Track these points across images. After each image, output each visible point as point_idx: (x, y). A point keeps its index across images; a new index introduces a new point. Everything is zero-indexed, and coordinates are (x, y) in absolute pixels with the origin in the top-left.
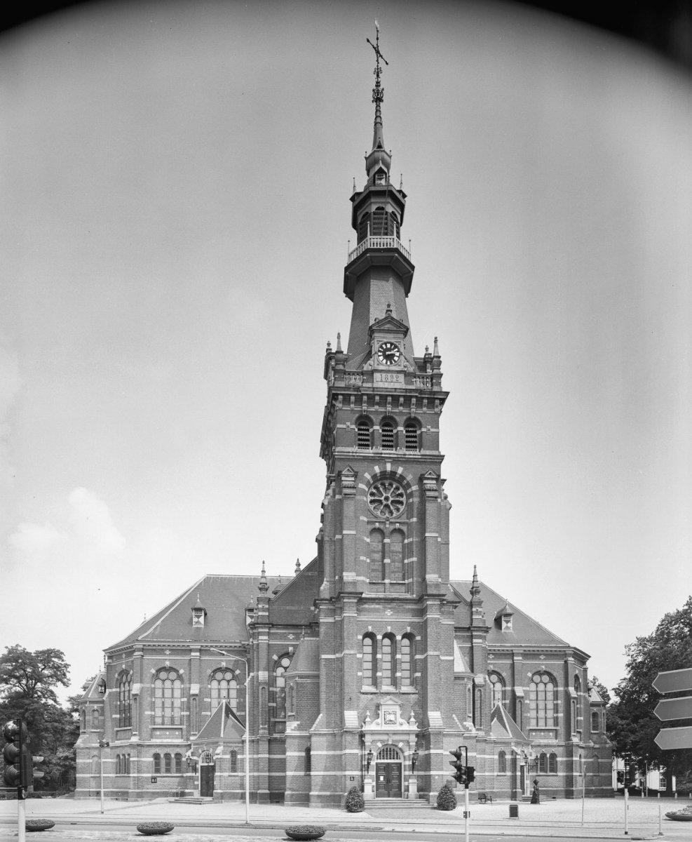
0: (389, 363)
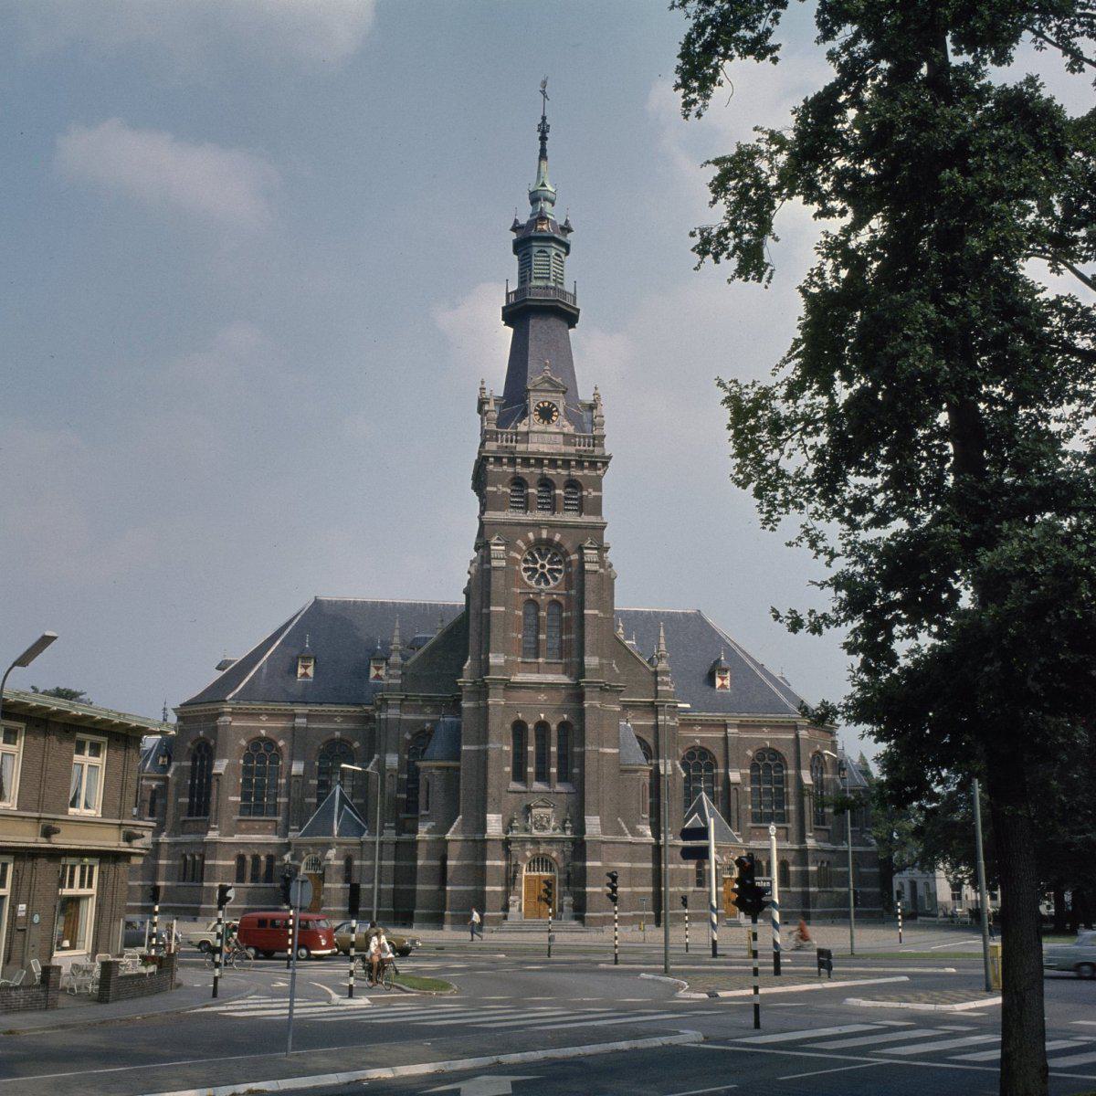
0: (546, 423)
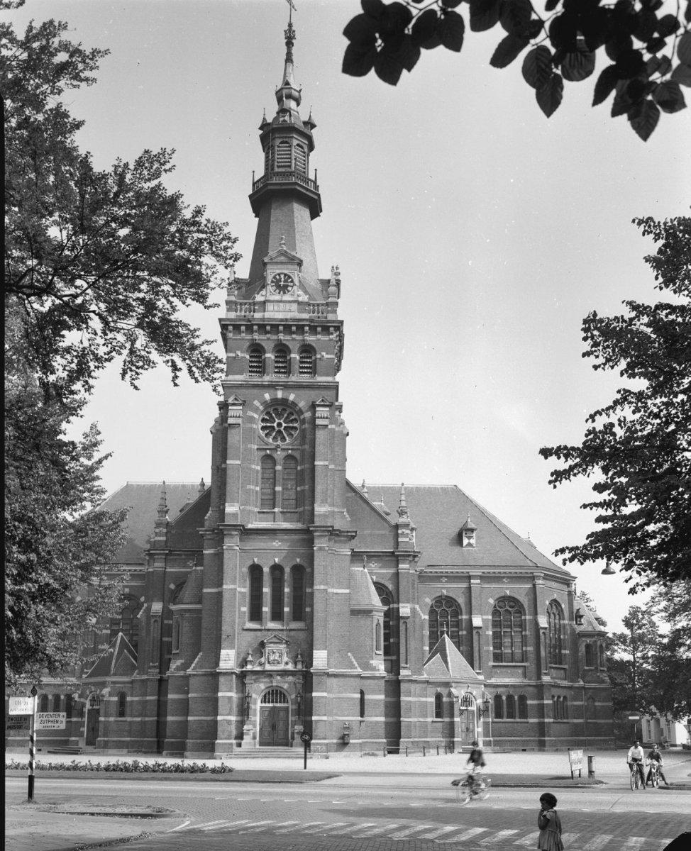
0: (281, 292)
